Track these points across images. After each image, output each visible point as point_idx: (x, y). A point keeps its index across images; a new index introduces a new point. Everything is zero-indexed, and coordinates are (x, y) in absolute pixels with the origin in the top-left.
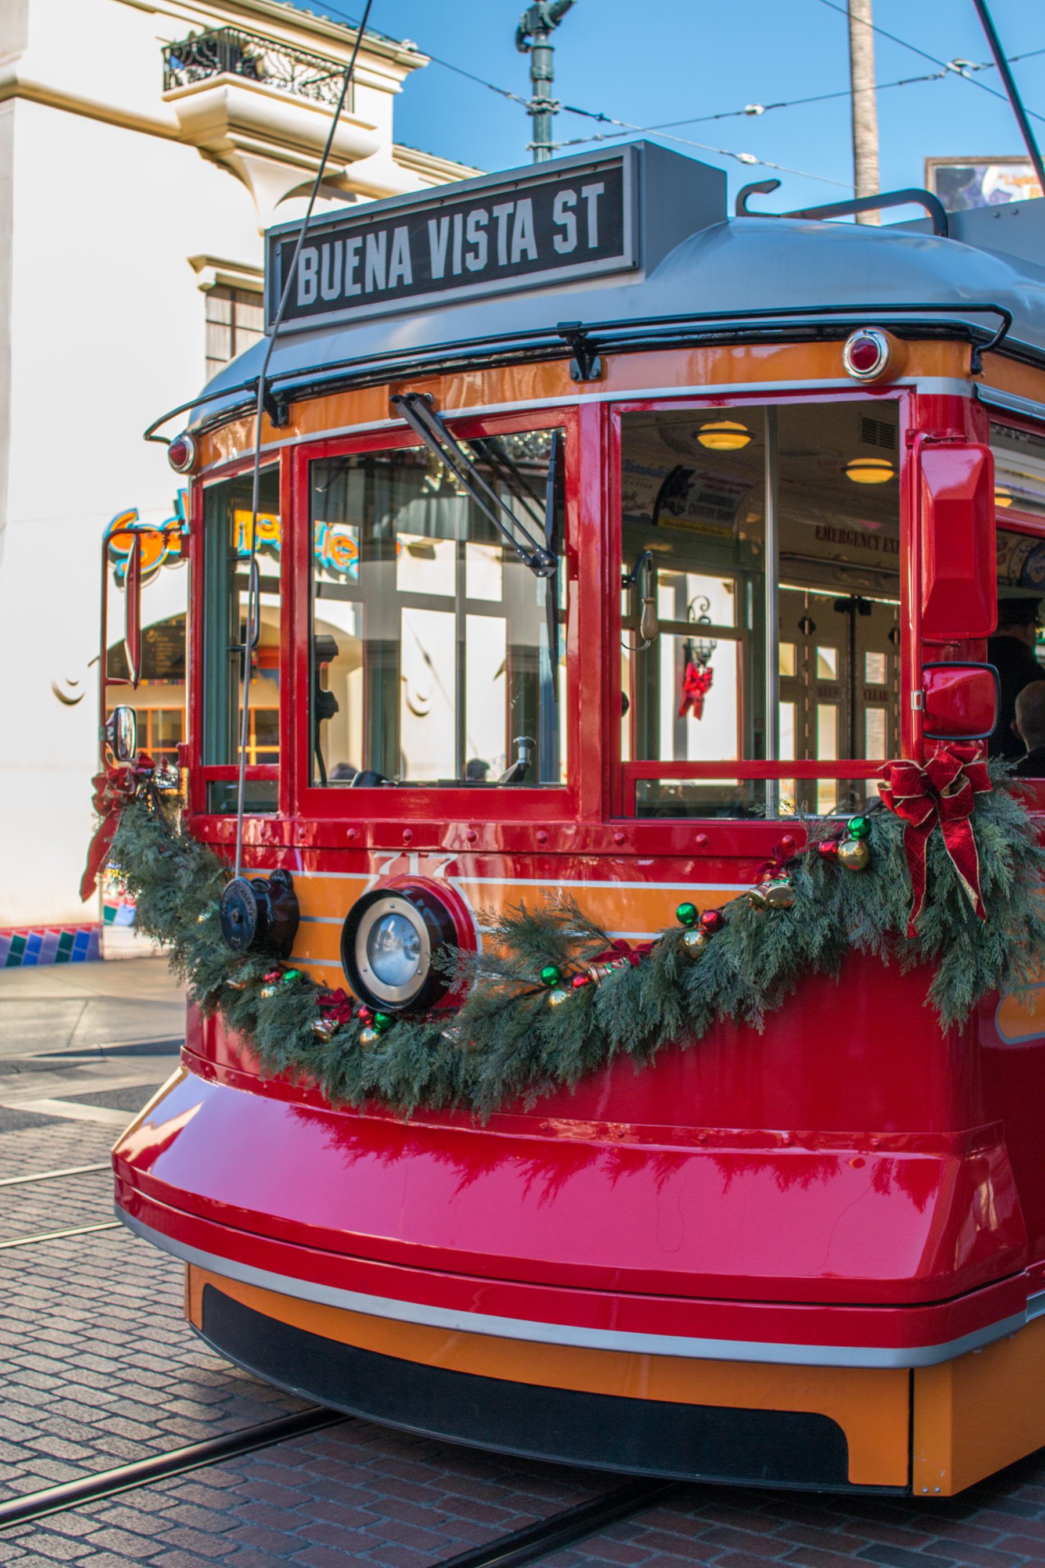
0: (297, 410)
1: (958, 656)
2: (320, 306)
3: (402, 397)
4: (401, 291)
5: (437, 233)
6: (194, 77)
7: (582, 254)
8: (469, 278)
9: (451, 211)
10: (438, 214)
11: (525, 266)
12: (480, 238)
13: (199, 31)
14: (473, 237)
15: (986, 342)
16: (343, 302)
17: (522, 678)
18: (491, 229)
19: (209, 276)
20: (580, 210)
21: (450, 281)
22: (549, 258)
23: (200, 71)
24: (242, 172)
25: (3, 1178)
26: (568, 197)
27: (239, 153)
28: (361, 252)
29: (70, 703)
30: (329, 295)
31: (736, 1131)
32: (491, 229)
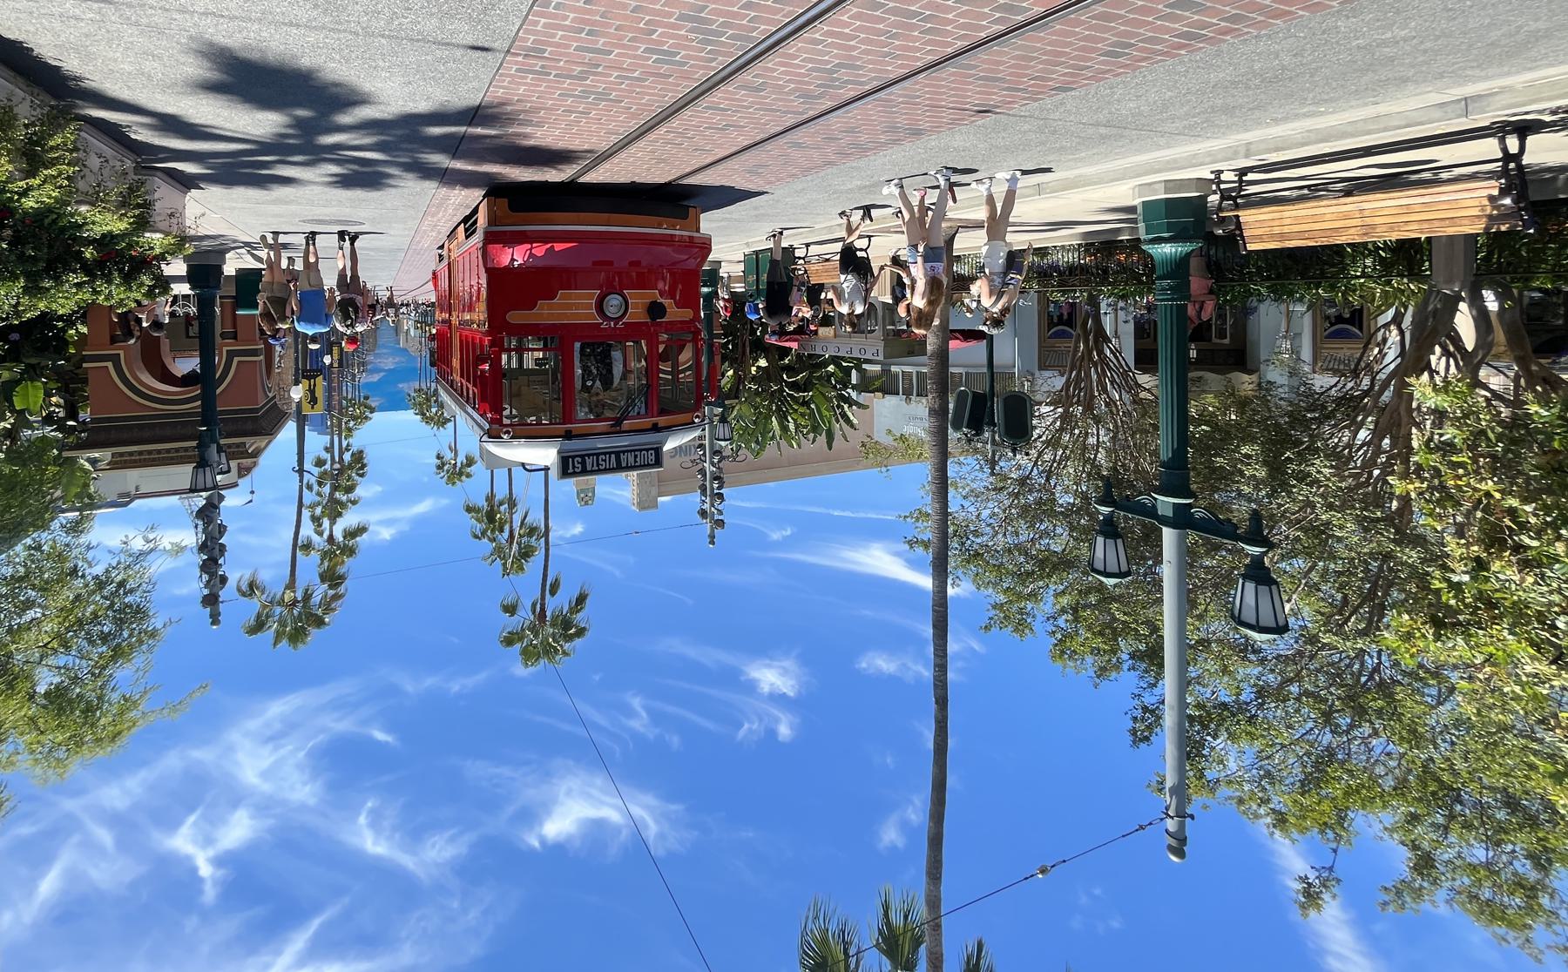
0: (650, 426)
1: (1554, 179)
3: (323, 517)
4: (624, 452)
8: (605, 454)
9: (609, 469)
10: (613, 469)
11: (589, 455)
12: (601, 462)
15: (899, 277)
16: (641, 450)
17: (765, 267)
21: (610, 453)
22: (582, 456)
28: (636, 462)
32: (598, 465)
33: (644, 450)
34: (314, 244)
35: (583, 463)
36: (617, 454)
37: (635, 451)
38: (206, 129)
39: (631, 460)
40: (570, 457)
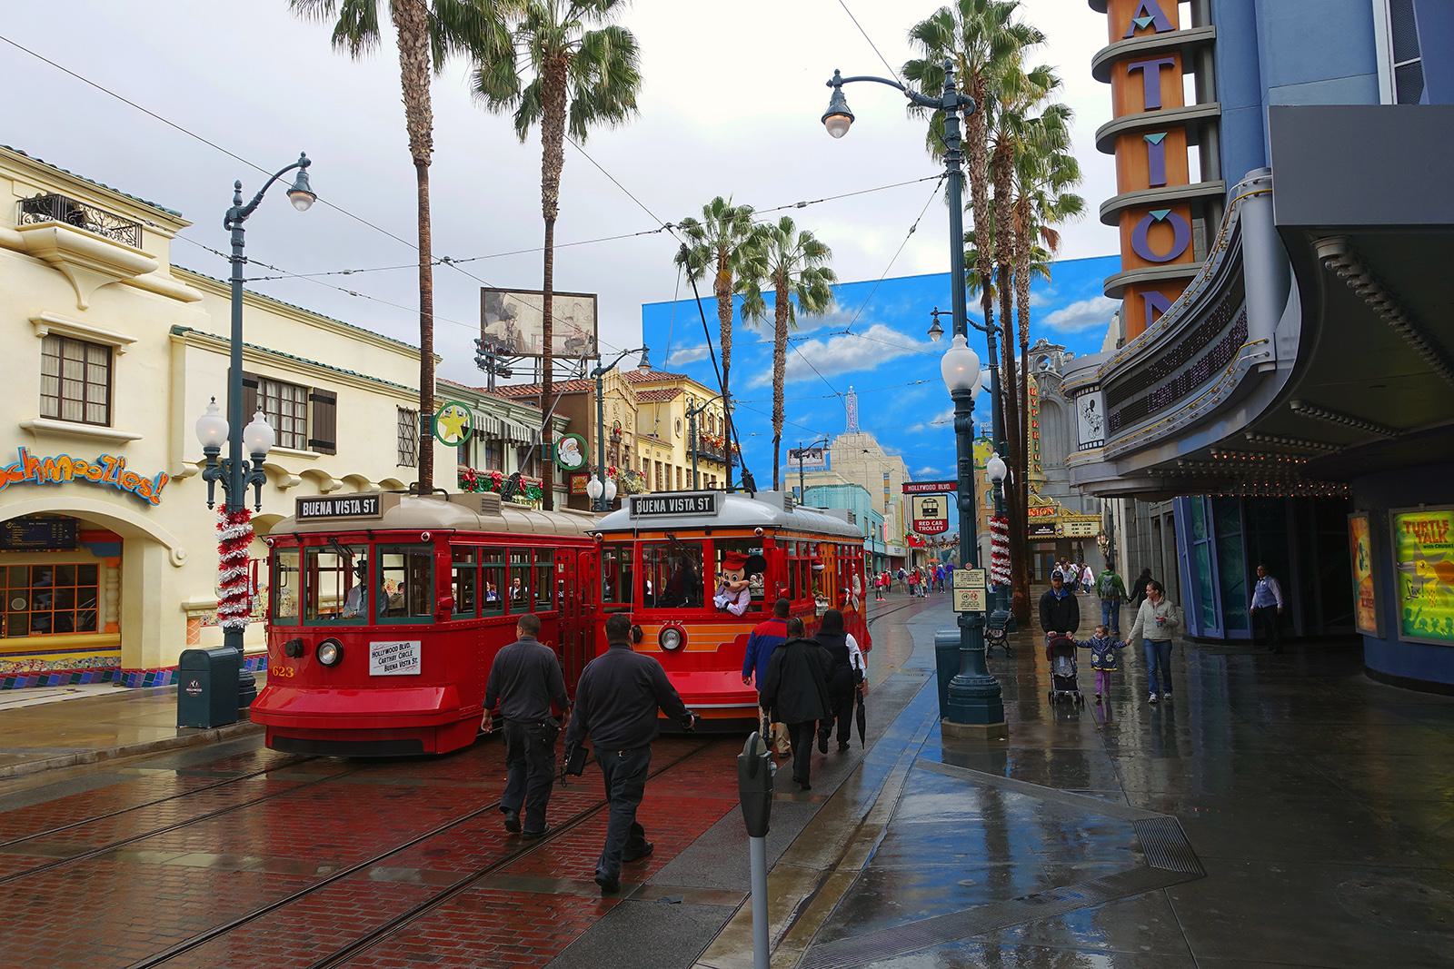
0: (713, 533)
2: (642, 513)
4: (663, 512)
5: (337, 505)
6: (37, 219)
7: (704, 510)
8: (679, 512)
11: (692, 511)
12: (682, 505)
13: (44, 194)
14: (346, 506)
16: (648, 513)
18: (350, 505)
19: (44, 330)
20: (704, 502)
22: (697, 510)
23: (42, 216)
24: (67, 273)
25: (8, 682)
26: (367, 501)
27: (66, 264)
28: (653, 504)
29: (178, 567)
30: (311, 514)
31: (1004, 403)
32: (684, 503)
33: (312, 516)
34: (188, 867)
35: (696, 505)
36: (668, 511)
37: (654, 513)
38: (856, 706)
39: (656, 505)
40: (372, 514)
